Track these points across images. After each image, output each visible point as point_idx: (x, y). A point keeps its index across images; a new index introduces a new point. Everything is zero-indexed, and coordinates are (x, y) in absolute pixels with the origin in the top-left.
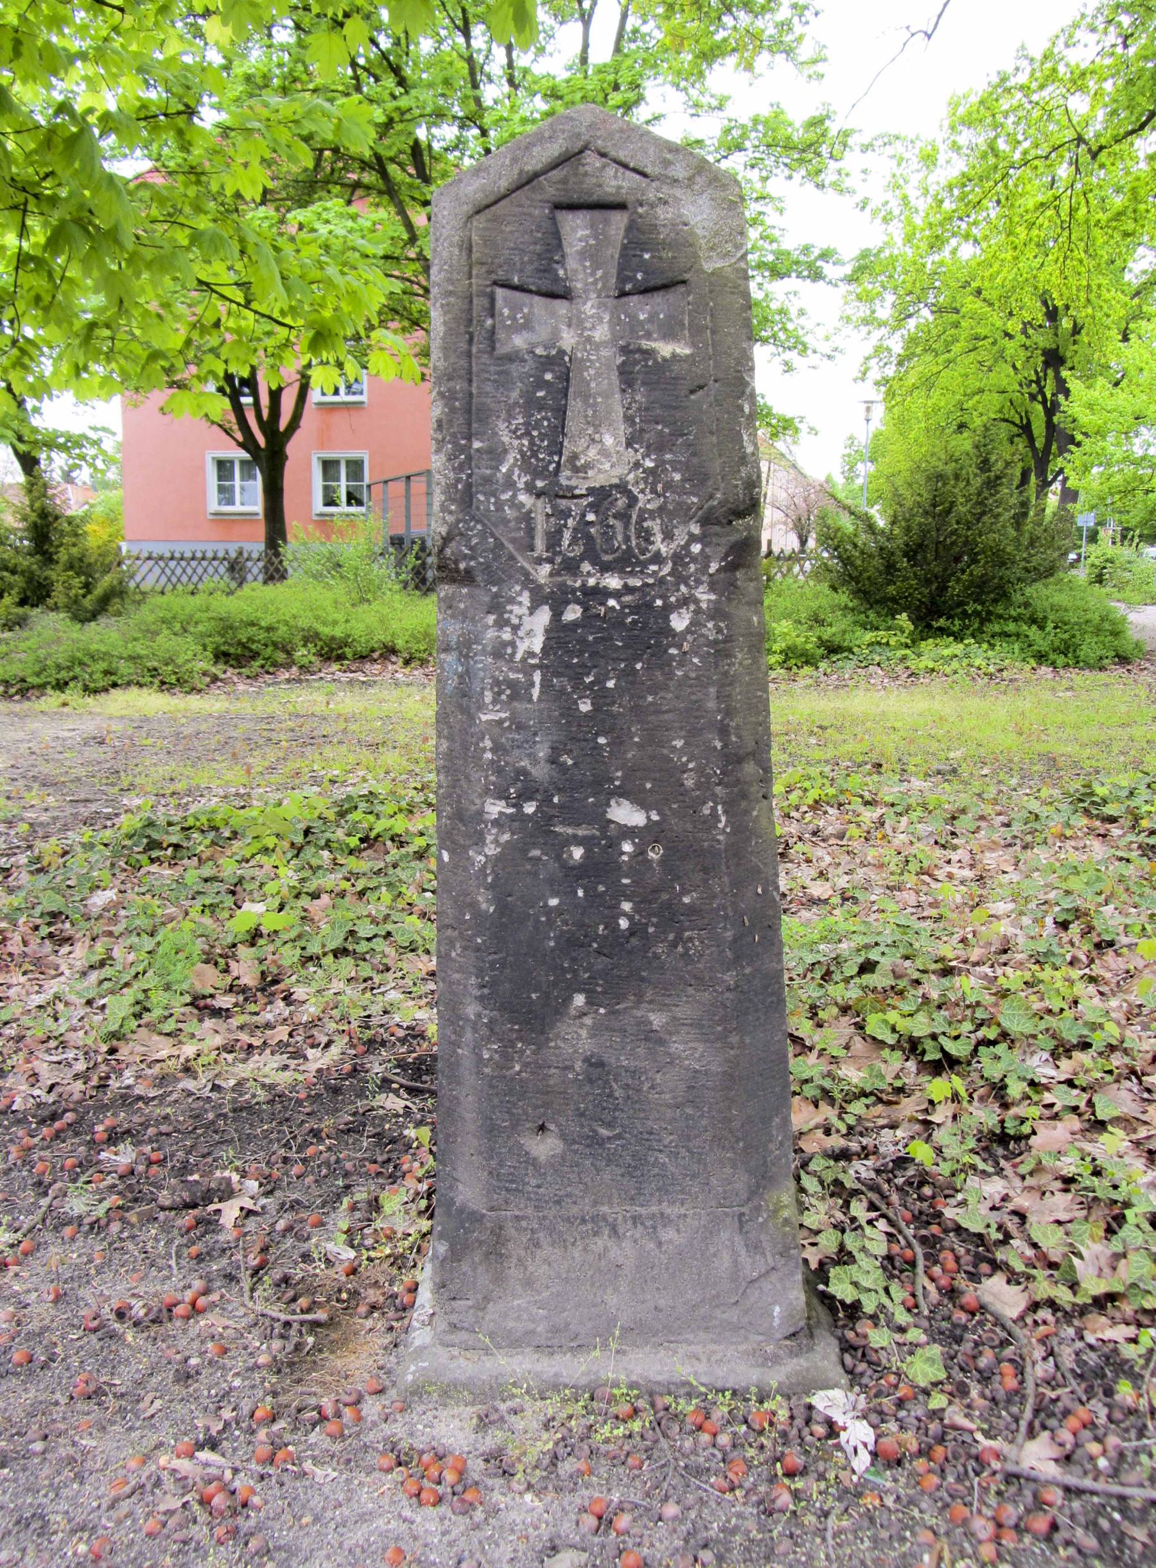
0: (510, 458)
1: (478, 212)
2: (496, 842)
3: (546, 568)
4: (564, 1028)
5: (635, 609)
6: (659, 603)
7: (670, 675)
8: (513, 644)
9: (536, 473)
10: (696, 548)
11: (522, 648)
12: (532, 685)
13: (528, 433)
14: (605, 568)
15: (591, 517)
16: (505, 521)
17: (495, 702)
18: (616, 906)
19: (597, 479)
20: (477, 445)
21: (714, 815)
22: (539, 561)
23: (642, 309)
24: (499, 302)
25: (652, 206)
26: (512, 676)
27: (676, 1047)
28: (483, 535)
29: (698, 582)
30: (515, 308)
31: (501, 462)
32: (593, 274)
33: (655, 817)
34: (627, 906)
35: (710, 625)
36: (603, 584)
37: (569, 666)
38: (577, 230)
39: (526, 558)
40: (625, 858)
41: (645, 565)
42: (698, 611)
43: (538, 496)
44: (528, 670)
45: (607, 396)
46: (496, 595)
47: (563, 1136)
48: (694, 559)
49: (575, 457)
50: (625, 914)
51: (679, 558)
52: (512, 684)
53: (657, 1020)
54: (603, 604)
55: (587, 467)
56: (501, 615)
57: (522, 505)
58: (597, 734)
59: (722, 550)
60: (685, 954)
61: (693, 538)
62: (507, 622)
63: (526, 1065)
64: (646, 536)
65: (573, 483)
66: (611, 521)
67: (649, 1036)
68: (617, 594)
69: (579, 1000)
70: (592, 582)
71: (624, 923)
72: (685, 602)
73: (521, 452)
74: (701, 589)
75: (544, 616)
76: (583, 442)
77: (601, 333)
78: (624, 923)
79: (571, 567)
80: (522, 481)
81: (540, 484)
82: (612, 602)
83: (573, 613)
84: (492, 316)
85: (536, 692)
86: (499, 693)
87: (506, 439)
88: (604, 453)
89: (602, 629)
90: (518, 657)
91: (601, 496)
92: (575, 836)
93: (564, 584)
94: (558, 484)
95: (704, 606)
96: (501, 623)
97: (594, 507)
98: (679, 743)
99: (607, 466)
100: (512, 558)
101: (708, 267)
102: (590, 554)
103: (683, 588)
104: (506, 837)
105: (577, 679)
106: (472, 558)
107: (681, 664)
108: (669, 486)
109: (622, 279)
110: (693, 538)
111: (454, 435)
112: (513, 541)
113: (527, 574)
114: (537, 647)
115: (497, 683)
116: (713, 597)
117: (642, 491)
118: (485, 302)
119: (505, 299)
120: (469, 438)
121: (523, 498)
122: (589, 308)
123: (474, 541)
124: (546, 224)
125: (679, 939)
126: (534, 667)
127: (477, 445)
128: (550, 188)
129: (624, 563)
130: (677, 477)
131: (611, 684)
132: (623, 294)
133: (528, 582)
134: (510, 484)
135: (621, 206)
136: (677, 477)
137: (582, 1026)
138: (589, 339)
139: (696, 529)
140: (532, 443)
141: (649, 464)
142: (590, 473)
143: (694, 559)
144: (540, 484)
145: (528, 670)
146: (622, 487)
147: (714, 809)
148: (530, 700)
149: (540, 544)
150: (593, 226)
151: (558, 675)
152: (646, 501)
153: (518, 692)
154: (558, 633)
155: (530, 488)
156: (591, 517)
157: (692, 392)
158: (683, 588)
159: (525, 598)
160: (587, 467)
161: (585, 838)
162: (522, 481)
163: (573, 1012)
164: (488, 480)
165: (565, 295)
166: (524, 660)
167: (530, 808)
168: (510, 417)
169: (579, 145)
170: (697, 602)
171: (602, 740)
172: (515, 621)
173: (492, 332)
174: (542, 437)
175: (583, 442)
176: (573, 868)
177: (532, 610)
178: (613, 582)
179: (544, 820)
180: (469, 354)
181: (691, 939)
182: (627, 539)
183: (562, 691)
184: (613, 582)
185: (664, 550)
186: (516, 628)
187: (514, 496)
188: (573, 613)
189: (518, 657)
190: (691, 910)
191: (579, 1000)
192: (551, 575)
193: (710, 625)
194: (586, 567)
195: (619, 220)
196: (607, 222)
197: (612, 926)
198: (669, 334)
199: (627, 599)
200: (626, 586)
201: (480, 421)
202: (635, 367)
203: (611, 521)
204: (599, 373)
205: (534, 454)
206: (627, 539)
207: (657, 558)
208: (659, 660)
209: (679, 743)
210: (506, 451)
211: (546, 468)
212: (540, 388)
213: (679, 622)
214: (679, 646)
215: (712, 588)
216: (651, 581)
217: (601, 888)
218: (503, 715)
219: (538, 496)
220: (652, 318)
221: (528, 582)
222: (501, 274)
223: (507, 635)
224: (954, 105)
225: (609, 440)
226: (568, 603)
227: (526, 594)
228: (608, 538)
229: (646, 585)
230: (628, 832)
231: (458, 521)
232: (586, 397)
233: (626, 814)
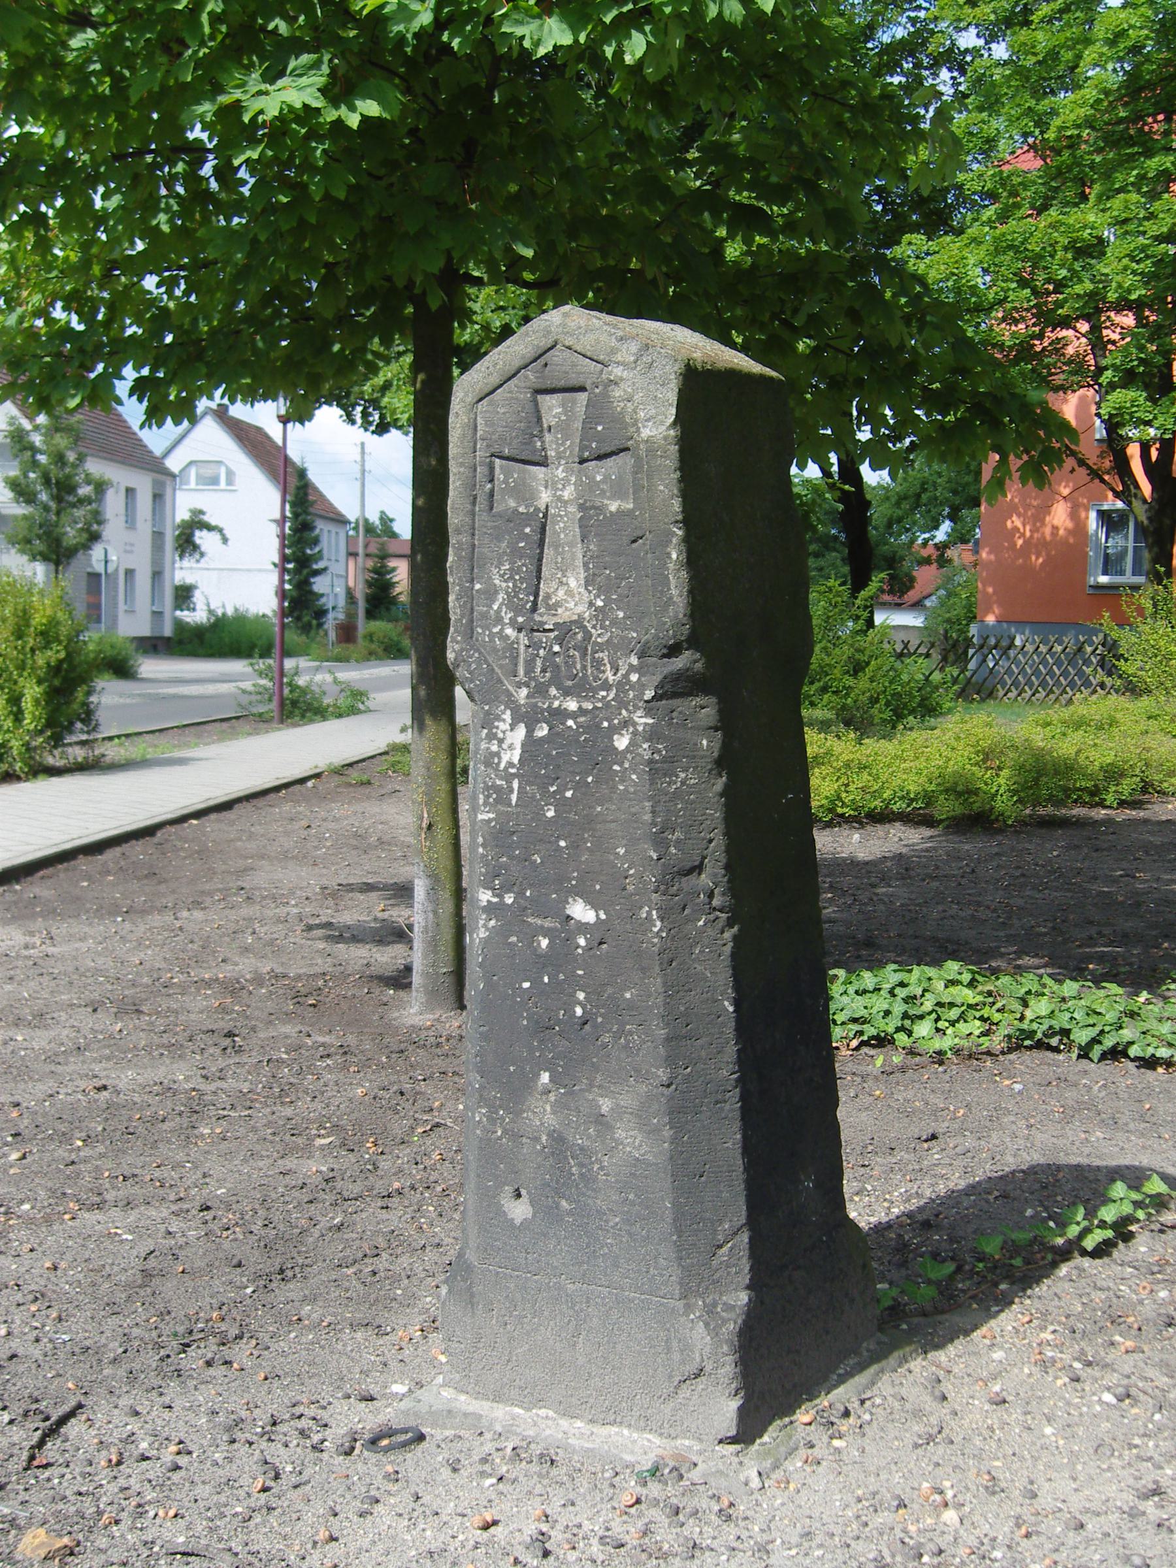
0: (501, 596)
1: (481, 400)
2: (485, 926)
3: (524, 692)
4: (533, 1102)
5: (587, 728)
6: (606, 724)
7: (614, 787)
8: (498, 754)
9: (518, 611)
10: (634, 677)
11: (505, 758)
12: (512, 791)
13: (511, 578)
14: (567, 692)
15: (556, 648)
16: (495, 650)
17: (486, 804)
18: (573, 995)
19: (563, 615)
20: (478, 586)
21: (649, 916)
22: (519, 685)
23: (599, 472)
24: (497, 470)
25: (606, 386)
26: (498, 782)
27: (620, 1134)
28: (478, 662)
29: (636, 708)
30: (508, 474)
31: (494, 602)
32: (563, 444)
33: (603, 917)
34: (581, 996)
35: (645, 746)
36: (565, 705)
37: (538, 776)
38: (552, 407)
39: (511, 683)
40: (580, 951)
41: (595, 691)
42: (635, 733)
43: (520, 630)
44: (509, 778)
45: (572, 545)
46: (488, 713)
47: (532, 1203)
48: (632, 687)
49: (548, 597)
50: (580, 1003)
51: (620, 685)
52: (498, 789)
53: (605, 1105)
54: (564, 724)
55: (558, 604)
56: (490, 730)
57: (508, 637)
58: (558, 838)
59: (657, 678)
60: (626, 1047)
61: (632, 669)
62: (495, 737)
63: (505, 1132)
64: (598, 665)
65: (545, 619)
66: (572, 652)
67: (599, 1119)
68: (573, 715)
69: (545, 1077)
70: (556, 704)
71: (579, 1011)
72: (626, 723)
73: (507, 593)
74: (639, 713)
75: (521, 731)
76: (554, 585)
77: (568, 493)
78: (579, 1011)
79: (540, 690)
80: (507, 616)
81: (520, 619)
82: (570, 723)
83: (542, 731)
84: (491, 481)
85: (514, 797)
86: (488, 797)
87: (497, 582)
88: (570, 593)
89: (562, 746)
90: (502, 766)
91: (565, 631)
92: (542, 927)
93: (535, 705)
94: (533, 619)
95: (640, 728)
96: (491, 737)
97: (560, 641)
98: (621, 851)
99: (572, 605)
100: (500, 681)
101: (646, 433)
102: (556, 681)
103: (624, 712)
104: (492, 923)
105: (544, 788)
106: (472, 681)
107: (622, 781)
108: (615, 622)
109: (582, 448)
110: (632, 669)
111: (460, 579)
112: (501, 667)
113: (510, 695)
114: (516, 760)
115: (487, 788)
116: (650, 721)
117: (594, 627)
118: (486, 470)
119: (501, 467)
120: (472, 581)
121: (509, 631)
122: (560, 473)
123: (474, 666)
124: (529, 407)
125: (621, 1033)
126: (514, 775)
127: (478, 586)
128: (530, 376)
129: (580, 689)
130: (621, 614)
131: (569, 794)
132: (582, 461)
133: (512, 704)
134: (499, 620)
135: (582, 389)
136: (621, 614)
137: (547, 1101)
138: (559, 499)
139: (634, 660)
140: (515, 586)
141: (600, 603)
142: (560, 611)
143: (632, 687)
144: (520, 619)
145: (509, 778)
146: (579, 623)
147: (649, 913)
148: (510, 805)
149: (521, 672)
150: (563, 405)
151: (531, 784)
152: (599, 636)
153: (502, 796)
154: (530, 745)
155: (513, 622)
156: (556, 648)
157: (634, 541)
158: (624, 712)
159: (507, 716)
160: (558, 604)
161: (549, 929)
162: (507, 616)
163: (540, 1088)
164: (485, 616)
165: (543, 463)
166: (506, 768)
167: (509, 899)
168: (500, 564)
169: (550, 343)
170: (635, 724)
171: (562, 844)
172: (501, 735)
173: (491, 494)
174: (522, 580)
175: (554, 585)
176: (540, 956)
177: (513, 727)
178: (572, 705)
179: (520, 910)
180: (473, 514)
181: (631, 1033)
182: (584, 667)
183: (533, 797)
184: (572, 705)
185: (611, 678)
186: (501, 741)
187: (502, 630)
188: (542, 731)
189: (502, 766)
190: (631, 1005)
191: (545, 1077)
192: (528, 697)
193: (645, 746)
194: (553, 691)
195: (583, 397)
196: (574, 402)
197: (570, 1012)
198: (618, 494)
199: (582, 719)
200: (580, 708)
201: (479, 567)
202: (591, 521)
203: (572, 652)
204: (564, 527)
205: (516, 596)
206: (584, 667)
207: (606, 686)
208: (605, 778)
209: (621, 851)
210: (496, 592)
211: (524, 606)
212: (522, 540)
213: (622, 742)
214: (621, 764)
215: (649, 712)
216: (600, 705)
217: (562, 977)
218: (492, 816)
219: (520, 630)
220: (606, 478)
221: (512, 704)
222: (496, 448)
223: (494, 748)
224: (392, 520)
225: (573, 583)
226: (539, 721)
227: (508, 712)
228: (570, 666)
229: (595, 708)
230: (583, 928)
231: (462, 650)
232: (556, 546)
233: (581, 912)
